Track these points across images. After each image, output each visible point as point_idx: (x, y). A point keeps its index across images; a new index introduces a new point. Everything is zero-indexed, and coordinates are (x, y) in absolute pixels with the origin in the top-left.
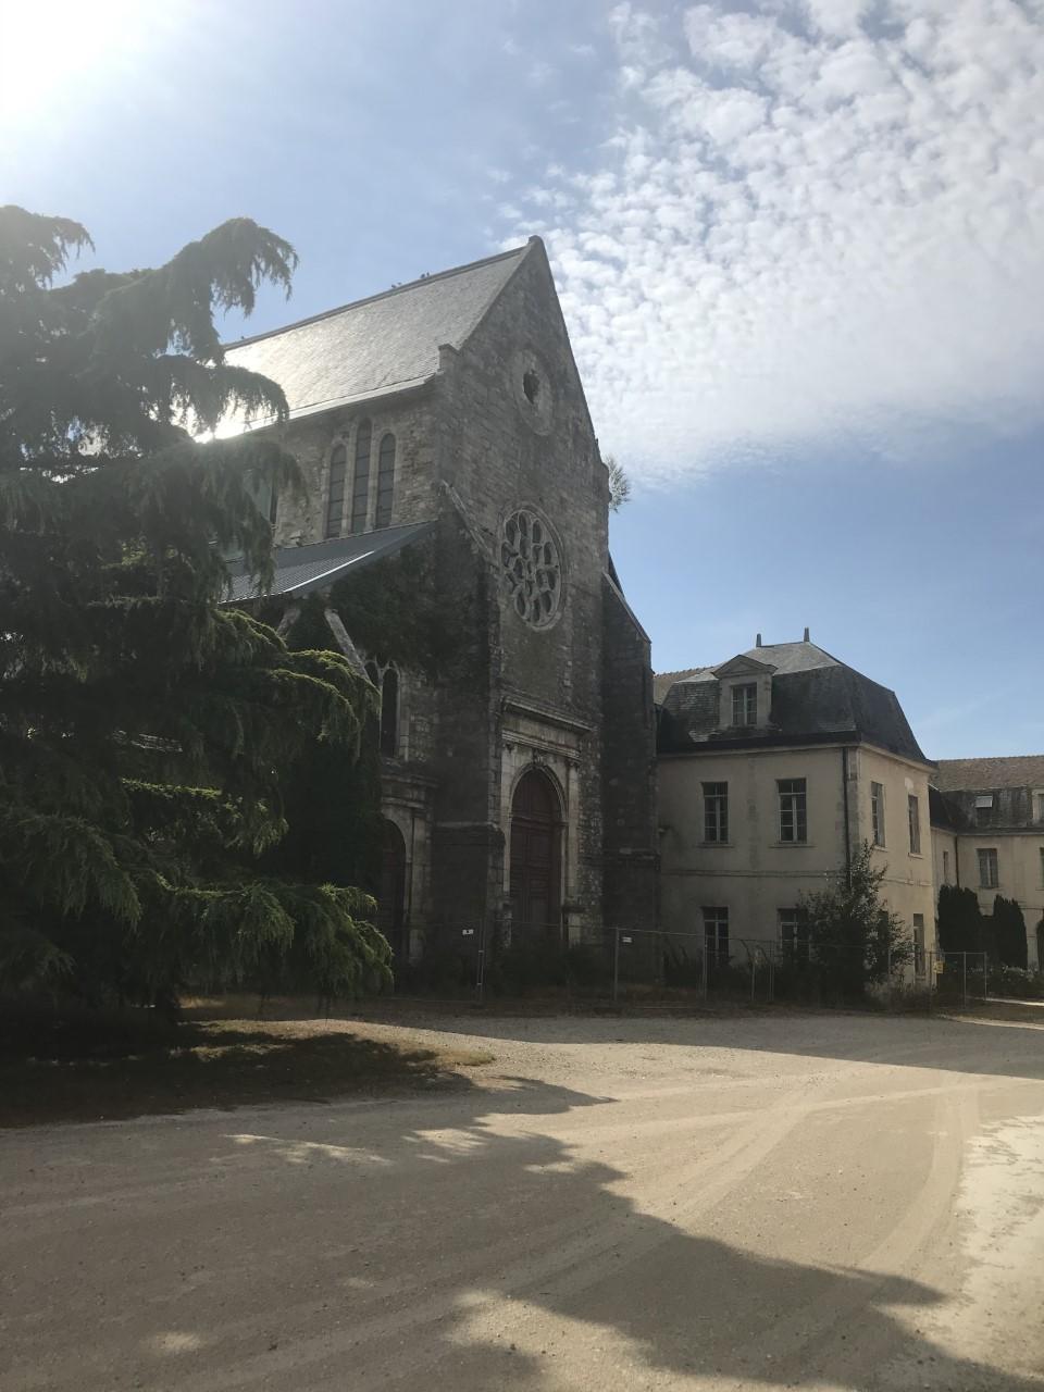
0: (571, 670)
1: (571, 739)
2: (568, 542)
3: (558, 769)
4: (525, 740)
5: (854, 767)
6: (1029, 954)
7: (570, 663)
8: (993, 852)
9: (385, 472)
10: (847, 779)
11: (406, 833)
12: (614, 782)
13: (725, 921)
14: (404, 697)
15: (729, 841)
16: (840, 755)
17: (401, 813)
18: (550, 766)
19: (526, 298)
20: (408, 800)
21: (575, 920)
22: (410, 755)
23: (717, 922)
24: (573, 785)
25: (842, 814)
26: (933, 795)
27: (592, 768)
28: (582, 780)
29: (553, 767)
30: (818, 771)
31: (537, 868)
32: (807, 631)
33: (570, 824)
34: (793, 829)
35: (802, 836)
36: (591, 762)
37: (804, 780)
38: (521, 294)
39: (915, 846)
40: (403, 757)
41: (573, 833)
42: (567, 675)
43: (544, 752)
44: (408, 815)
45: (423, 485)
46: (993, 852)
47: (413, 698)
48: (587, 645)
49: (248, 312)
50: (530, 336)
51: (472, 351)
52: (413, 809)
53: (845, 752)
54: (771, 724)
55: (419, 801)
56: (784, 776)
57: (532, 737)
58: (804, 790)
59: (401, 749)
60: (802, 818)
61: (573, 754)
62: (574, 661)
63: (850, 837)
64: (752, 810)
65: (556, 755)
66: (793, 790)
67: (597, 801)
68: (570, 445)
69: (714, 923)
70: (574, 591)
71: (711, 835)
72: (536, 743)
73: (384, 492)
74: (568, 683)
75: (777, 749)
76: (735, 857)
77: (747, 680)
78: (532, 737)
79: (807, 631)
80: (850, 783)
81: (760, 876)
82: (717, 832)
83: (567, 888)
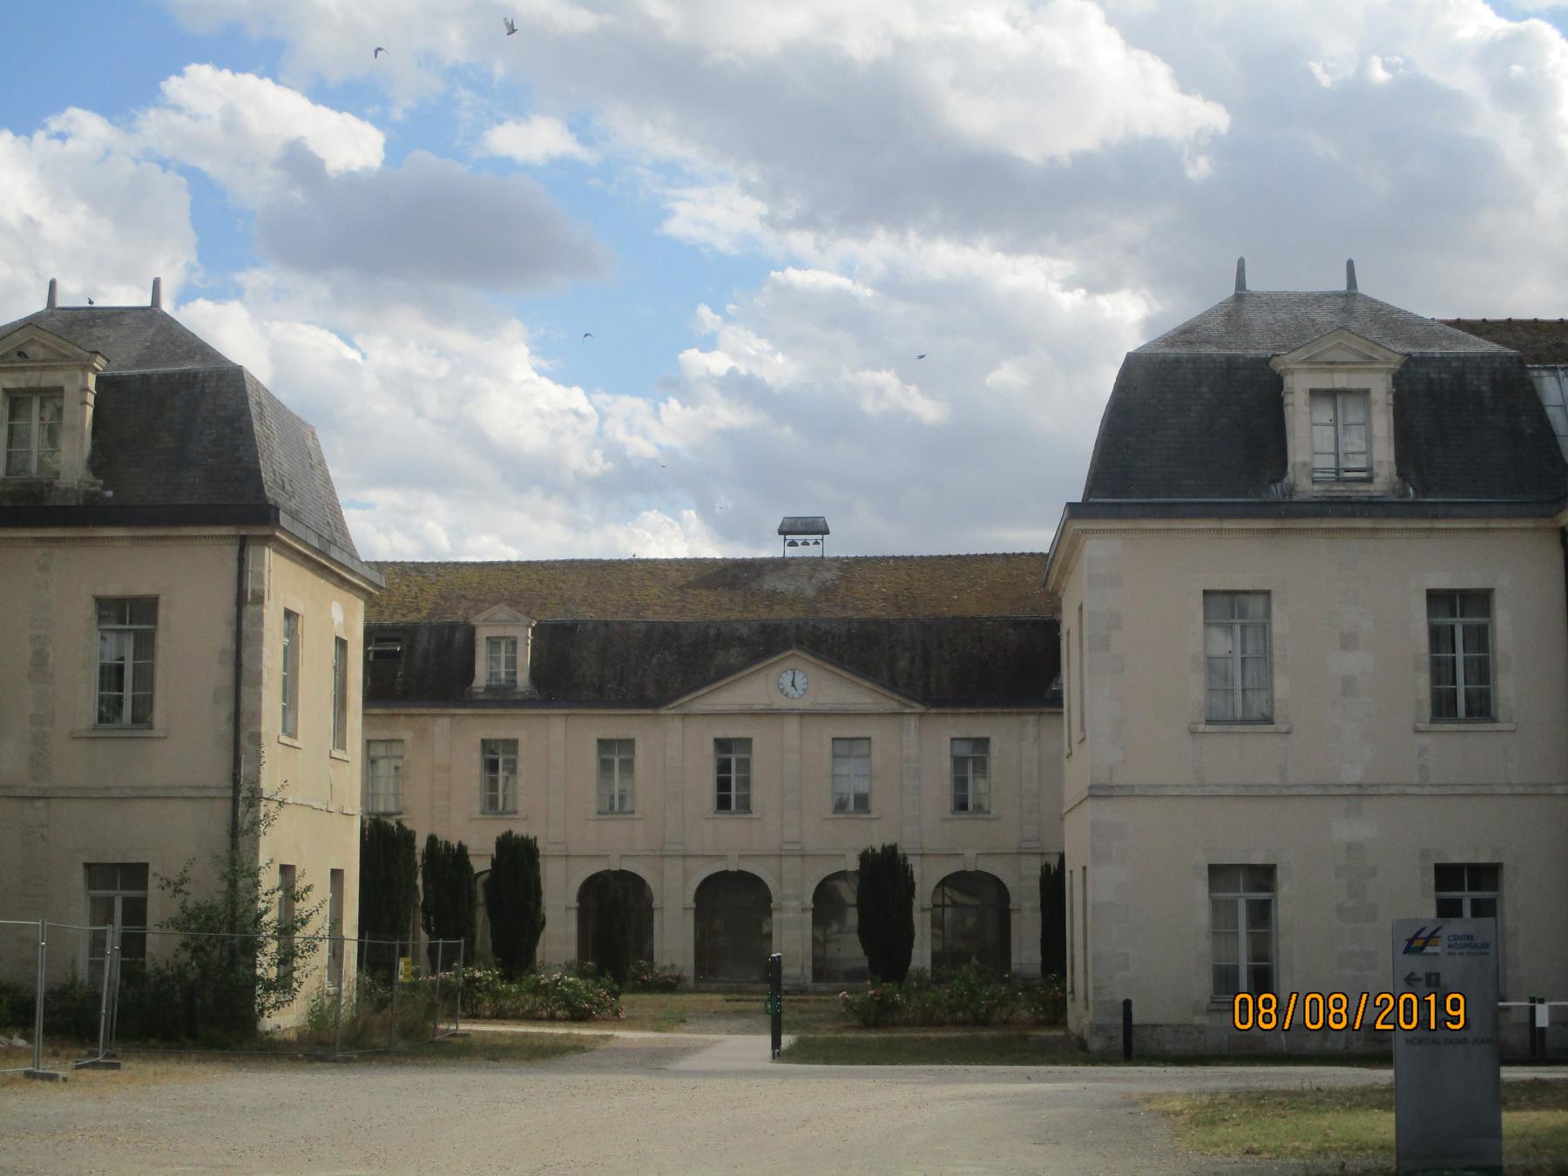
5: (260, 578)
6: (915, 952)
8: (628, 744)
10: (245, 600)
13: (1487, 894)
15: (1501, 716)
16: (232, 551)
23: (119, 897)
25: (229, 671)
26: (373, 634)
30: (180, 575)
32: (1350, 266)
34: (125, 699)
35: (142, 717)
39: (340, 740)
46: (628, 744)
53: (243, 542)
54: (90, 477)
56: (114, 589)
58: (154, 621)
63: (244, 719)
66: (132, 615)
71: (109, 711)
75: (175, 532)
77: (48, 379)
79: (1350, 266)
80: (249, 610)
81: (48, 798)
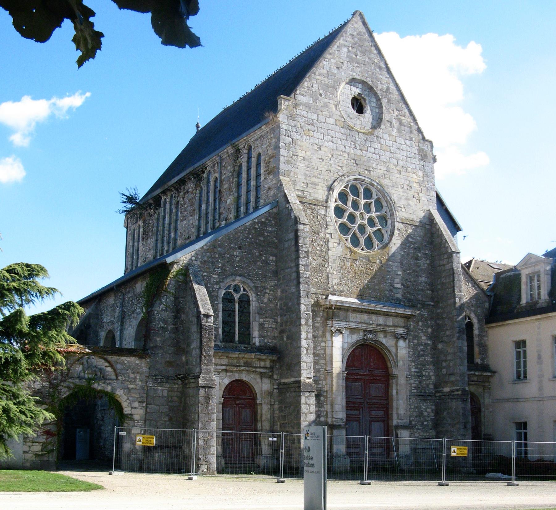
0: (400, 277)
1: (401, 321)
2: (395, 195)
3: (387, 341)
4: (353, 325)
7: (400, 273)
9: (258, 176)
11: (257, 389)
12: (440, 346)
14: (254, 308)
17: (252, 376)
18: (381, 340)
19: (349, 51)
20: (256, 367)
21: (404, 435)
22: (260, 342)
24: (401, 352)
27: (424, 338)
28: (414, 349)
29: (384, 341)
31: (229, 419)
33: (399, 376)
35: (525, 377)
36: (421, 334)
37: (460, 230)
38: (345, 50)
40: (254, 344)
41: (402, 380)
42: (397, 281)
43: (370, 332)
44: (258, 377)
45: (272, 180)
47: (261, 308)
48: (417, 258)
49: (81, 62)
50: (354, 74)
51: (302, 94)
52: (261, 373)
55: (264, 368)
57: (361, 323)
59: (254, 339)
60: (525, 362)
61: (401, 331)
62: (404, 271)
64: (539, 357)
65: (385, 332)
67: (428, 359)
68: (395, 133)
69: (510, 444)
70: (401, 226)
71: (519, 377)
72: (365, 326)
73: (257, 188)
74: (399, 286)
76: (530, 389)
78: (361, 323)
82: (521, 376)
83: (397, 414)
